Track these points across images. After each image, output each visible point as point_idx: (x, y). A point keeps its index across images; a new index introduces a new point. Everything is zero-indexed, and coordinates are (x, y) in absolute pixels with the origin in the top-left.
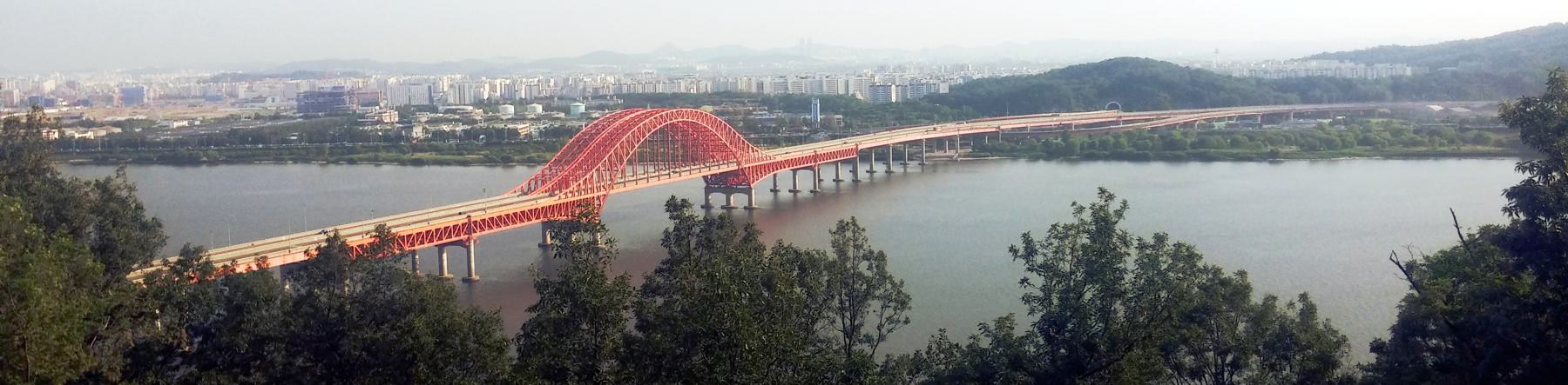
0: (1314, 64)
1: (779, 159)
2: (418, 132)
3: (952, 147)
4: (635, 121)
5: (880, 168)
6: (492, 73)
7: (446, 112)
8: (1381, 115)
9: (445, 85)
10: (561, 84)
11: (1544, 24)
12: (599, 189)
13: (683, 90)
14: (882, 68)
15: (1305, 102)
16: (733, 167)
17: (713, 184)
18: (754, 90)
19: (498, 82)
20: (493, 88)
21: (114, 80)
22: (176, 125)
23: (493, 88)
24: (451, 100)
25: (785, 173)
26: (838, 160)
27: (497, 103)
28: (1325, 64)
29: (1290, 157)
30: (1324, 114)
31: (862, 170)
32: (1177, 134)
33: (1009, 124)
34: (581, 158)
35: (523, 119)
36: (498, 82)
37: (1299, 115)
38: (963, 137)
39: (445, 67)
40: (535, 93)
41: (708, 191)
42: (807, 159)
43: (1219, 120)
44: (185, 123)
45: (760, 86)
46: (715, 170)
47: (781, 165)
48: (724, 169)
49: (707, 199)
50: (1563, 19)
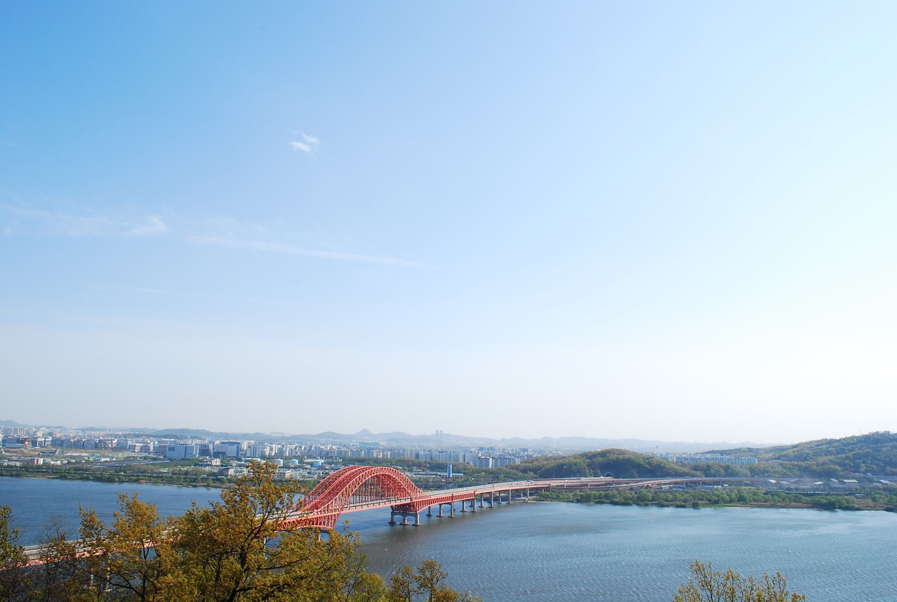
0: (709, 456)
1: (433, 497)
2: (231, 472)
3: (525, 495)
4: (357, 473)
5: (485, 505)
6: (271, 441)
7: (246, 461)
8: (746, 485)
9: (245, 446)
10: (308, 449)
11: (819, 439)
12: (335, 510)
13: (375, 456)
14: (481, 449)
15: (706, 476)
16: (408, 501)
17: (395, 510)
18: (414, 458)
19: (274, 446)
20: (271, 449)
21: (428, 430)
22: (103, 460)
23: (271, 449)
24: (248, 455)
25: (435, 506)
26: (465, 499)
27: (273, 458)
28: (715, 456)
29: (704, 506)
30: (717, 483)
31: (477, 505)
32: (644, 491)
33: (554, 483)
34: (327, 492)
35: (288, 468)
36: (274, 446)
37: (704, 483)
38: (531, 489)
39: (246, 436)
40: (294, 454)
41: (393, 514)
42: (447, 498)
43: (665, 484)
44: (108, 459)
45: (417, 456)
46: (398, 503)
47: (434, 501)
48: (403, 502)
49: (392, 519)
50: (896, 428)
